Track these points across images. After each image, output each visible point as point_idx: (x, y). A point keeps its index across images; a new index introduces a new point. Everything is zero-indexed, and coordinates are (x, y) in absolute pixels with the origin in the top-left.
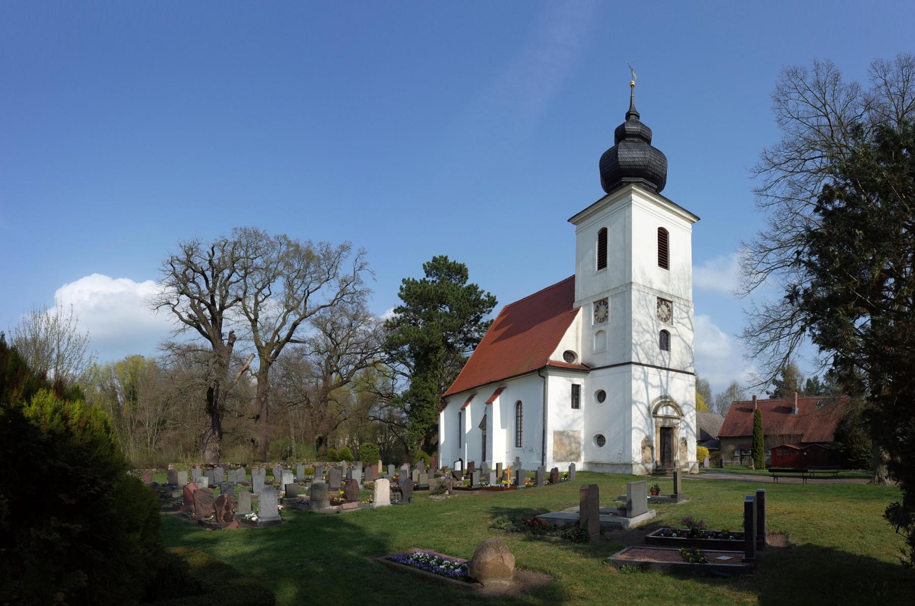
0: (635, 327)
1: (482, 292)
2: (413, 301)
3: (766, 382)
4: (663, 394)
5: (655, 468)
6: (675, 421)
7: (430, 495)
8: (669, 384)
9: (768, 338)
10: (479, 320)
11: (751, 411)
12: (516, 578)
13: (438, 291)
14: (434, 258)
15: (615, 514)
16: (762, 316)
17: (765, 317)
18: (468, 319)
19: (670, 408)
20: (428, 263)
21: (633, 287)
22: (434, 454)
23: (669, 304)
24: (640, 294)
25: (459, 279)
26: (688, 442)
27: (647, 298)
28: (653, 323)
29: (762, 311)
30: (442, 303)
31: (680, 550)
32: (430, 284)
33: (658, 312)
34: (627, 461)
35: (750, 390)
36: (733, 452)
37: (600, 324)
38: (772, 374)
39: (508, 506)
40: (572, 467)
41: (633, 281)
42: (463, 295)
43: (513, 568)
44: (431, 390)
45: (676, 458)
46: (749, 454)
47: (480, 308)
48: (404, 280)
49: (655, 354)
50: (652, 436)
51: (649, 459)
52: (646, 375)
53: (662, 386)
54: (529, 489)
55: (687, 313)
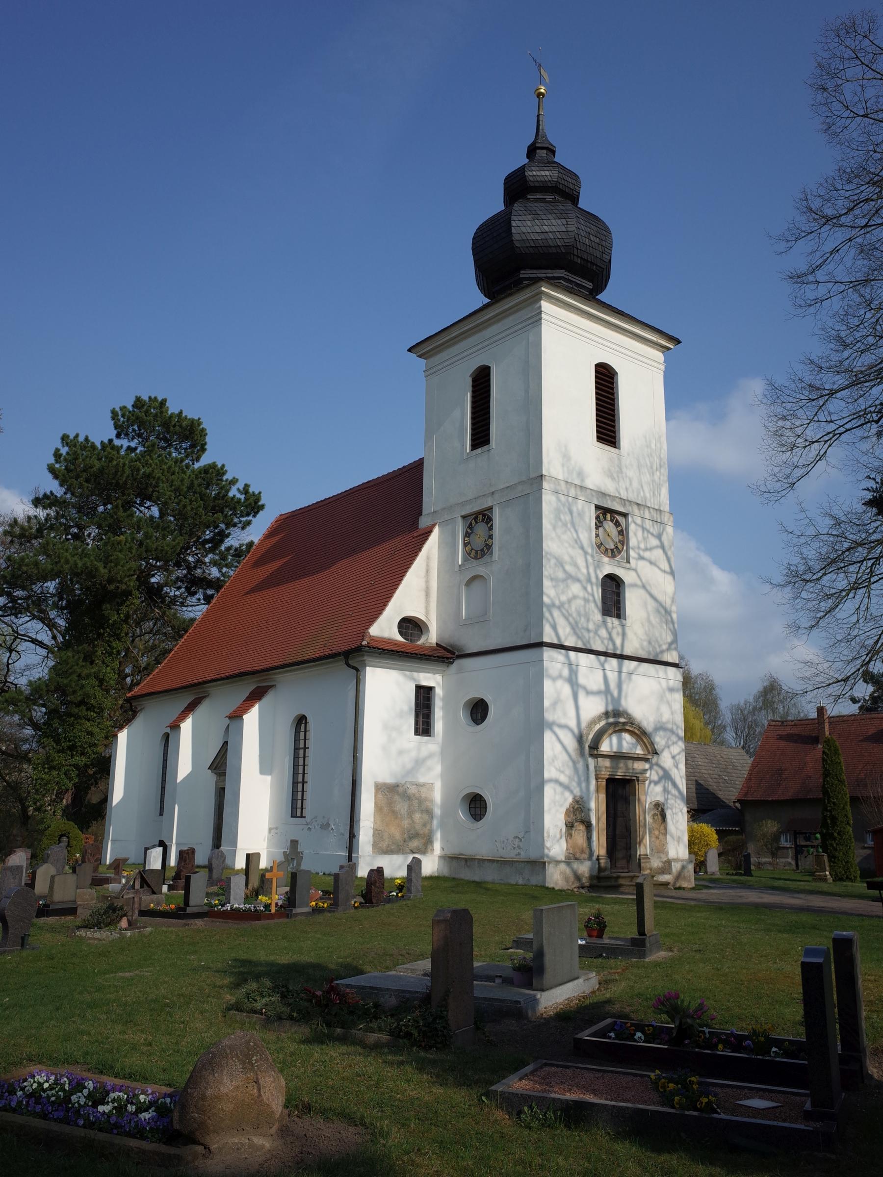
0: (548, 570)
1: (234, 482)
2: (81, 486)
3: (846, 680)
4: (610, 708)
5: (595, 873)
6: (639, 766)
7: (79, 928)
8: (624, 687)
9: (841, 582)
10: (222, 541)
11: (815, 740)
12: (284, 1132)
13: (138, 470)
14: (138, 399)
15: (508, 981)
16: (825, 538)
17: (832, 539)
18: (199, 538)
19: (627, 737)
20: (123, 408)
21: (545, 485)
22: (94, 827)
23: (621, 519)
24: (559, 500)
25: (186, 449)
26: (669, 814)
27: (574, 509)
28: (586, 561)
29: (825, 524)
30: (145, 496)
31: (652, 1075)
32: (122, 452)
33: (597, 536)
34: (533, 855)
35: (809, 696)
36: (776, 838)
37: (475, 562)
38: (859, 662)
39: (272, 958)
40: (414, 867)
41: (544, 473)
42: (192, 483)
43: (280, 1109)
44: (101, 681)
45: (641, 851)
46: (816, 843)
47: (226, 516)
48: (64, 438)
49: (591, 626)
50: (589, 799)
51: (582, 852)
52: (573, 670)
53: (607, 691)
54: (320, 918)
55: (659, 537)
